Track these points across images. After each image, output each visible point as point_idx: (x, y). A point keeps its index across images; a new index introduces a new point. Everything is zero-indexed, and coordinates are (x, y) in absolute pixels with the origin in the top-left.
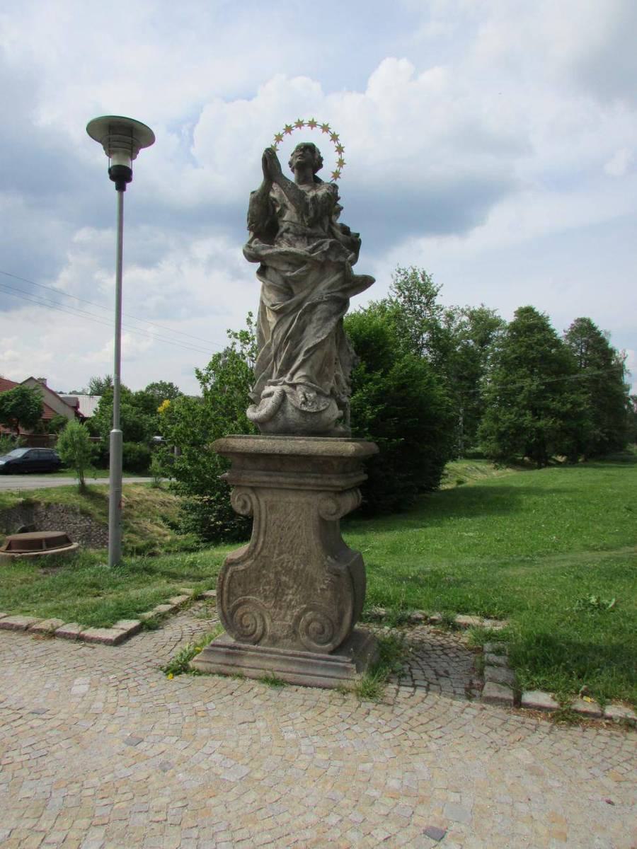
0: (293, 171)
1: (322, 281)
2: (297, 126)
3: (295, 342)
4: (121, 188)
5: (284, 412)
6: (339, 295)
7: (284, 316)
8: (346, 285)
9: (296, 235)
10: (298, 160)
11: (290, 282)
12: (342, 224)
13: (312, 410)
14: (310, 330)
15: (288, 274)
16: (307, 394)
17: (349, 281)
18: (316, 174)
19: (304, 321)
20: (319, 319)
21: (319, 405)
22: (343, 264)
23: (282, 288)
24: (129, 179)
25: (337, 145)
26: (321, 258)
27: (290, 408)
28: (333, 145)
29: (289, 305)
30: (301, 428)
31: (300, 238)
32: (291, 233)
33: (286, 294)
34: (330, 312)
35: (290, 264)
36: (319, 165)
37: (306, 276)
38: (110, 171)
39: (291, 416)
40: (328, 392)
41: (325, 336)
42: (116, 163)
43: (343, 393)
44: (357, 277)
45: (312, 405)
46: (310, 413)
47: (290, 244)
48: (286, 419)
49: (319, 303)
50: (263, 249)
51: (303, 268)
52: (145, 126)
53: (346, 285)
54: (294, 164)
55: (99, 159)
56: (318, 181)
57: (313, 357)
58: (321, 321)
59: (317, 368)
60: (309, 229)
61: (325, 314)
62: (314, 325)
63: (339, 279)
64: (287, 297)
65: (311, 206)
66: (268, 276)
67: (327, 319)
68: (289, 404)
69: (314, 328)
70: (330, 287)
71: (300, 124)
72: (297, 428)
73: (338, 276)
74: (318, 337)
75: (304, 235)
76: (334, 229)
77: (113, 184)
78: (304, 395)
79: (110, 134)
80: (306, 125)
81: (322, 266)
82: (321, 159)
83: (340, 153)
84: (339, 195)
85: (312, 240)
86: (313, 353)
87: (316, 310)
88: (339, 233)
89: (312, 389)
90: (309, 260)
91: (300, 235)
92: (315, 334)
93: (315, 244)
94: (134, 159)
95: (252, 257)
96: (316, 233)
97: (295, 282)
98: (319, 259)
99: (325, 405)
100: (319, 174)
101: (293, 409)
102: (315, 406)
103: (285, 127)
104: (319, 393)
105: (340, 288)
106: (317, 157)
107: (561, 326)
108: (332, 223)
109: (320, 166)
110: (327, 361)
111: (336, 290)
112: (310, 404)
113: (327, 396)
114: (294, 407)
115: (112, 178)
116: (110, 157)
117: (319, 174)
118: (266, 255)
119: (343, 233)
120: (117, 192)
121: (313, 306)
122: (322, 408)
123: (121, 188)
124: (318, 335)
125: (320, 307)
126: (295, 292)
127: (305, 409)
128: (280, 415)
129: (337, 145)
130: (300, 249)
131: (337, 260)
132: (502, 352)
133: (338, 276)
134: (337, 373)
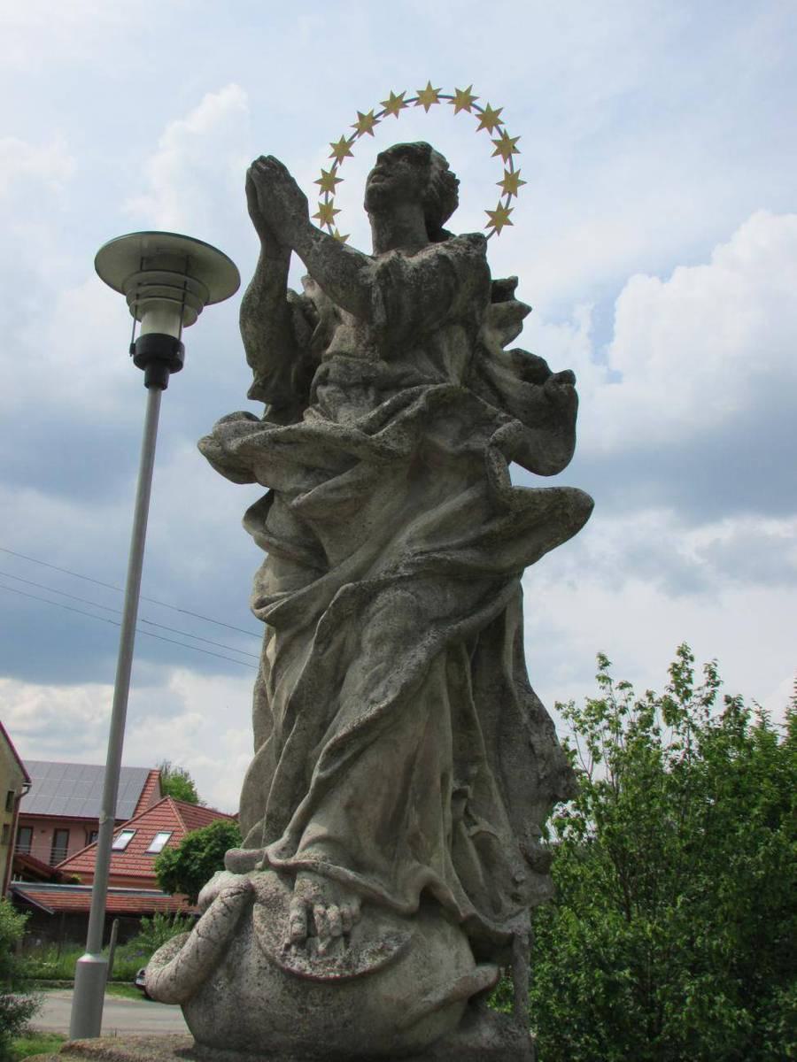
3: (315, 721)
4: (156, 382)
5: (233, 976)
6: (467, 557)
7: (294, 637)
8: (495, 526)
9: (344, 387)
13: (319, 973)
14: (356, 677)
16: (319, 909)
17: (505, 511)
19: (341, 650)
20: (378, 642)
21: (358, 950)
22: (477, 457)
23: (288, 546)
24: (177, 365)
25: (499, 138)
26: (400, 441)
27: (253, 959)
28: (487, 139)
29: (310, 597)
30: (295, 1038)
31: (354, 392)
32: (333, 382)
33: (303, 565)
34: (419, 613)
35: (309, 470)
37: (359, 505)
38: (133, 349)
39: (254, 992)
40: (411, 901)
41: (391, 697)
42: (150, 330)
43: (516, 898)
45: (330, 948)
46: (315, 981)
47: (328, 415)
48: (238, 999)
49: (384, 585)
52: (226, 257)
53: (495, 526)
55: (113, 322)
57: (358, 773)
58: (386, 648)
59: (374, 811)
60: (382, 366)
61: (396, 623)
62: (365, 660)
63: (469, 507)
64: (308, 575)
65: (376, 292)
66: (270, 523)
67: (406, 639)
68: (253, 946)
69: (365, 670)
70: (432, 534)
72: (278, 1038)
74: (373, 702)
75: (365, 384)
76: (497, 370)
77: (140, 375)
78: (309, 912)
79: (142, 270)
81: (419, 470)
83: (404, 105)
86: (357, 757)
87: (373, 609)
88: (510, 380)
89: (345, 889)
90: (356, 451)
91: (356, 385)
92: (367, 690)
94: (187, 325)
96: (404, 376)
97: (329, 525)
98: (393, 445)
99: (381, 951)
101: (264, 962)
102: (341, 955)
104: (372, 905)
105: (472, 534)
106: (434, 174)
107: (457, 178)
108: (480, 351)
110: (410, 787)
112: (321, 947)
113: (410, 916)
114: (265, 955)
115: (140, 361)
116: (137, 318)
120: (147, 390)
121: (364, 597)
122: (368, 963)
123: (156, 382)
124: (372, 696)
125: (382, 599)
126: (332, 559)
127: (298, 963)
128: (221, 985)
129: (499, 138)
132: (329, 612)
134: (484, 825)
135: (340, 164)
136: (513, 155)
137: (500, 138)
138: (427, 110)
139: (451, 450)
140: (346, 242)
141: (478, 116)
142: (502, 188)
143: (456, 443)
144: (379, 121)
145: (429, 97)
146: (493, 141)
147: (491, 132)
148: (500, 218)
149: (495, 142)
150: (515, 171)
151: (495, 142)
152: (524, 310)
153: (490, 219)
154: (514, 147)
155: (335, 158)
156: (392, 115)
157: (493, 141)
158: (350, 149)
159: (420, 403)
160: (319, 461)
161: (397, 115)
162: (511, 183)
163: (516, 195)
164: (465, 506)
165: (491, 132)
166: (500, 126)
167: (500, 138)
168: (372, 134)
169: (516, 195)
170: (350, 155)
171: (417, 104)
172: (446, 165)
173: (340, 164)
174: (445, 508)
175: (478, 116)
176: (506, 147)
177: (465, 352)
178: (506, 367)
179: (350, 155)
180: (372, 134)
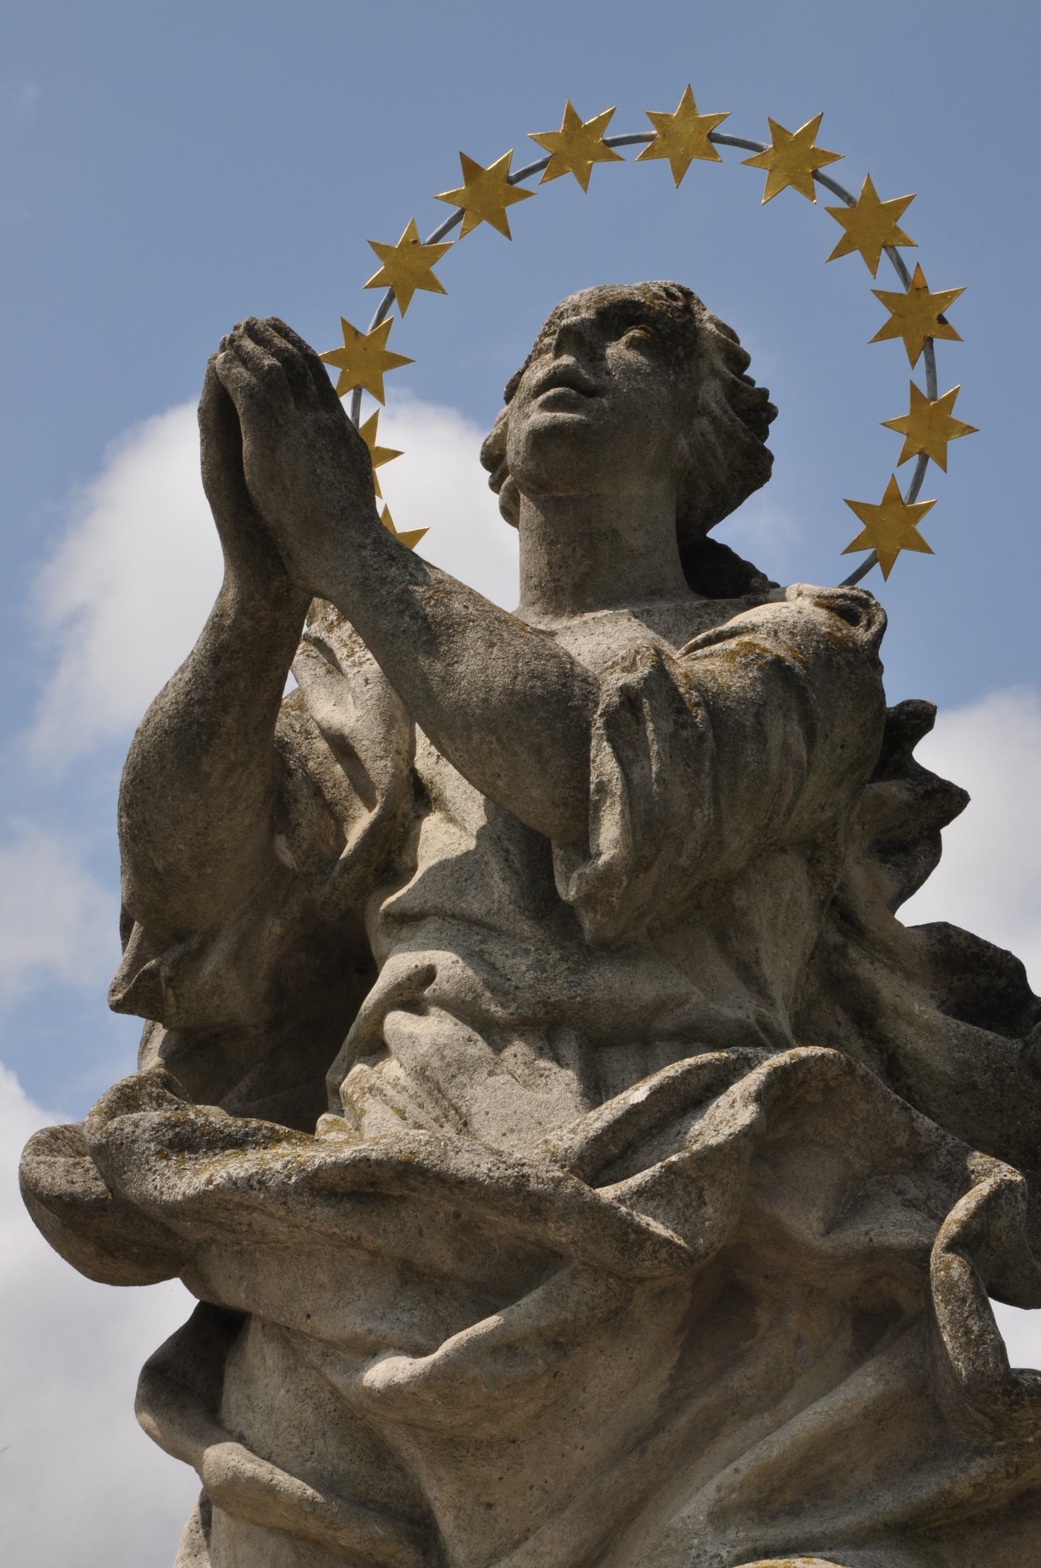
0: (510, 513)
1: (707, 1432)
2: (552, 167)
10: (539, 417)
11: (411, 1451)
12: (942, 935)
15: (389, 1370)
18: (719, 533)
25: (891, 282)
28: (860, 288)
36: (737, 449)
44: (1014, 1370)
50: (184, 1143)
51: (529, 1309)
53: (964, 1477)
54: (514, 453)
56: (738, 583)
63: (877, 1417)
71: (578, 148)
73: (863, 1386)
76: (888, 986)
80: (919, 375)
82: (764, 393)
84: (787, 594)
85: (615, 1060)
88: (919, 1014)
90: (559, 1233)
93: (638, 1094)
95: (99, 1225)
96: (661, 1006)
100: (742, 532)
103: (924, 528)
105: (888, 1503)
108: (850, 925)
109: (753, 470)
111: (847, 1521)
117: (742, 532)
118: (200, 1205)
119: (960, 1009)
129: (891, 282)
130: (531, 1118)
131: (855, 1235)
133: (863, 1386)
135: (403, 310)
136: (940, 345)
137: (897, 287)
138: (679, 174)
139: (825, 1245)
140: (417, 550)
141: (833, 212)
142: (899, 441)
143: (832, 1226)
144: (527, 194)
145: (686, 140)
146: (877, 293)
147: (873, 265)
148: (889, 528)
149: (886, 298)
150: (942, 395)
151: (886, 298)
152: (949, 800)
153: (860, 527)
154: (942, 320)
155: (385, 291)
156: (569, 178)
157: (877, 293)
158: (434, 269)
159: (730, 1114)
160: (438, 1252)
161: (584, 180)
162: (930, 427)
163: (943, 465)
164: (866, 1414)
165: (873, 265)
166: (902, 250)
167: (897, 287)
168: (925, 549)
169: (943, 465)
170: (432, 284)
171: (648, 154)
172: (740, 361)
173: (403, 310)
174: (810, 1420)
175: (833, 212)
176: (918, 320)
177: (807, 929)
178: (909, 976)
179: (432, 284)
180: (925, 549)
